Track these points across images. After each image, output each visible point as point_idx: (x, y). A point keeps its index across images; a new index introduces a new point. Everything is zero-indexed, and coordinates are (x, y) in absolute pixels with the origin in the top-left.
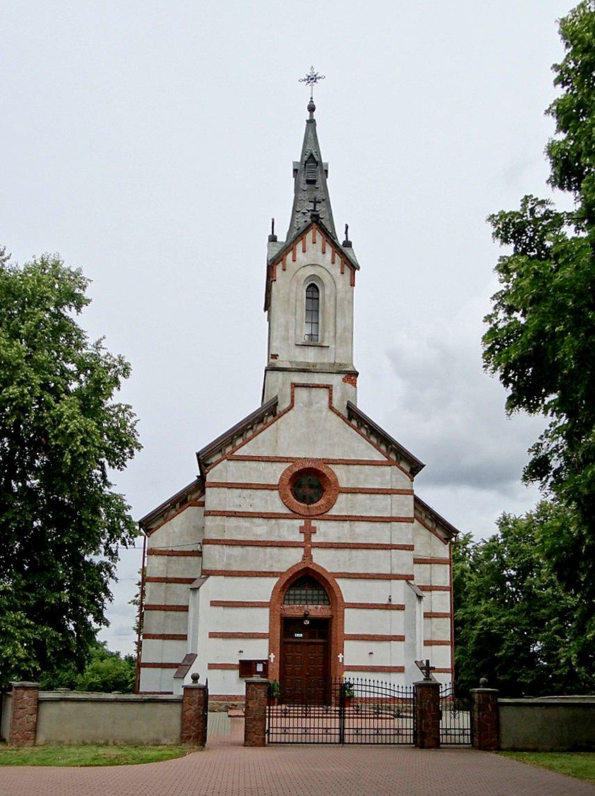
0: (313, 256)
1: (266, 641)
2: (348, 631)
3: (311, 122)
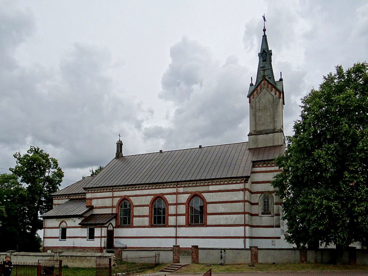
0: (267, 96)
1: (208, 212)
2: (135, 214)
3: (265, 37)
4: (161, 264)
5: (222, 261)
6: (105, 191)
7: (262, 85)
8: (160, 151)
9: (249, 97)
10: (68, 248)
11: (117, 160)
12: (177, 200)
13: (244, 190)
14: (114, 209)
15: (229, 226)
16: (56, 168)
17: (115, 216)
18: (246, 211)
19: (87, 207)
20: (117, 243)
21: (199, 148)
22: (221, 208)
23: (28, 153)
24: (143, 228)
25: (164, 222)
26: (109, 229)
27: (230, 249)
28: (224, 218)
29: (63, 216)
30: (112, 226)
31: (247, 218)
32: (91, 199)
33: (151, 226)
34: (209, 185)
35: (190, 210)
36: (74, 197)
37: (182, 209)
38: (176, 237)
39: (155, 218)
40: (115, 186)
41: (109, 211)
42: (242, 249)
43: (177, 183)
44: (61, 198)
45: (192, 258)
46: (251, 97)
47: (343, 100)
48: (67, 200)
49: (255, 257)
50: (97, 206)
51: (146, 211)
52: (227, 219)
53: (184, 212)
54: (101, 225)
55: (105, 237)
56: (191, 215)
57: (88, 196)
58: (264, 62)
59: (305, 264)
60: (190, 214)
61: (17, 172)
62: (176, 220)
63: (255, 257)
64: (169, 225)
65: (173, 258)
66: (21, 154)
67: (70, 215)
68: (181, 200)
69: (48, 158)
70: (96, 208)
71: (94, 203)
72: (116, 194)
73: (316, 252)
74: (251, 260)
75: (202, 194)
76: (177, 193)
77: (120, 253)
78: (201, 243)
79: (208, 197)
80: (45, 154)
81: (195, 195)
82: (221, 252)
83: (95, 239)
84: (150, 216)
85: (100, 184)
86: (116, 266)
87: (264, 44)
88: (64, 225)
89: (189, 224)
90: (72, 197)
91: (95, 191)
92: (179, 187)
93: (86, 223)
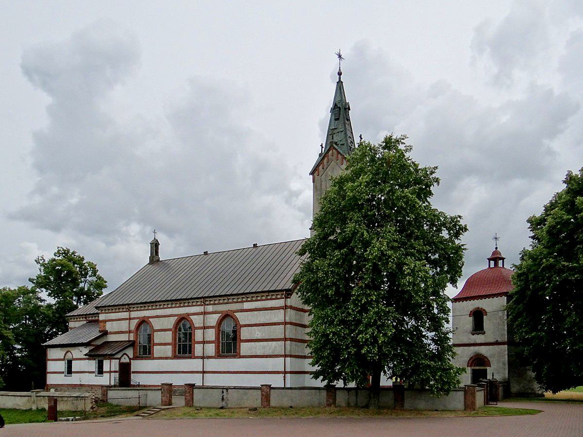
3: (340, 84)
4: (149, 407)
5: (224, 404)
6: (121, 310)
7: (330, 157)
8: (254, 245)
9: (312, 174)
10: (74, 387)
11: (151, 266)
12: (205, 322)
13: (286, 307)
14: (132, 335)
15: (267, 356)
16: (95, 275)
17: (132, 344)
18: (287, 337)
19: (100, 331)
20: (135, 379)
21: (254, 247)
22: (258, 333)
23: (54, 257)
24: (166, 359)
25: (190, 352)
26: (123, 360)
27: (235, 388)
28: (260, 346)
29: (67, 344)
30: (128, 357)
31: (288, 347)
32: (105, 321)
33: (175, 357)
34: (243, 302)
35: (221, 335)
36: (94, 318)
37: (211, 335)
38: (204, 372)
39: (179, 345)
40: (208, 297)
41: (124, 337)
42: (283, 388)
43: (204, 300)
44: (78, 319)
45: (186, 399)
46: (315, 174)
47: (352, 191)
48: (85, 322)
49: (266, 398)
50: (112, 331)
51: (168, 337)
52: (264, 347)
53: (213, 338)
54: (111, 357)
55: (115, 372)
56: (222, 343)
57: (102, 317)
58: (336, 122)
59: (333, 408)
60: (221, 342)
61: (42, 283)
62: (203, 349)
63: (266, 398)
64: (196, 355)
65: (162, 399)
66: (44, 258)
67: (75, 344)
68: (210, 322)
69: (84, 262)
70: (111, 333)
71: (109, 327)
72: (134, 314)
73: (348, 392)
74: (262, 403)
75: (190, 316)
76: (205, 313)
77: (106, 393)
78: (197, 380)
79: (242, 318)
80: (79, 258)
81: (226, 316)
82: (223, 392)
83: (104, 374)
84: (217, 341)
85: (181, 295)
86: (94, 409)
87: (338, 94)
88: (69, 356)
89: (219, 355)
90: (90, 318)
91: (110, 311)
92: (207, 305)
93: (93, 354)
